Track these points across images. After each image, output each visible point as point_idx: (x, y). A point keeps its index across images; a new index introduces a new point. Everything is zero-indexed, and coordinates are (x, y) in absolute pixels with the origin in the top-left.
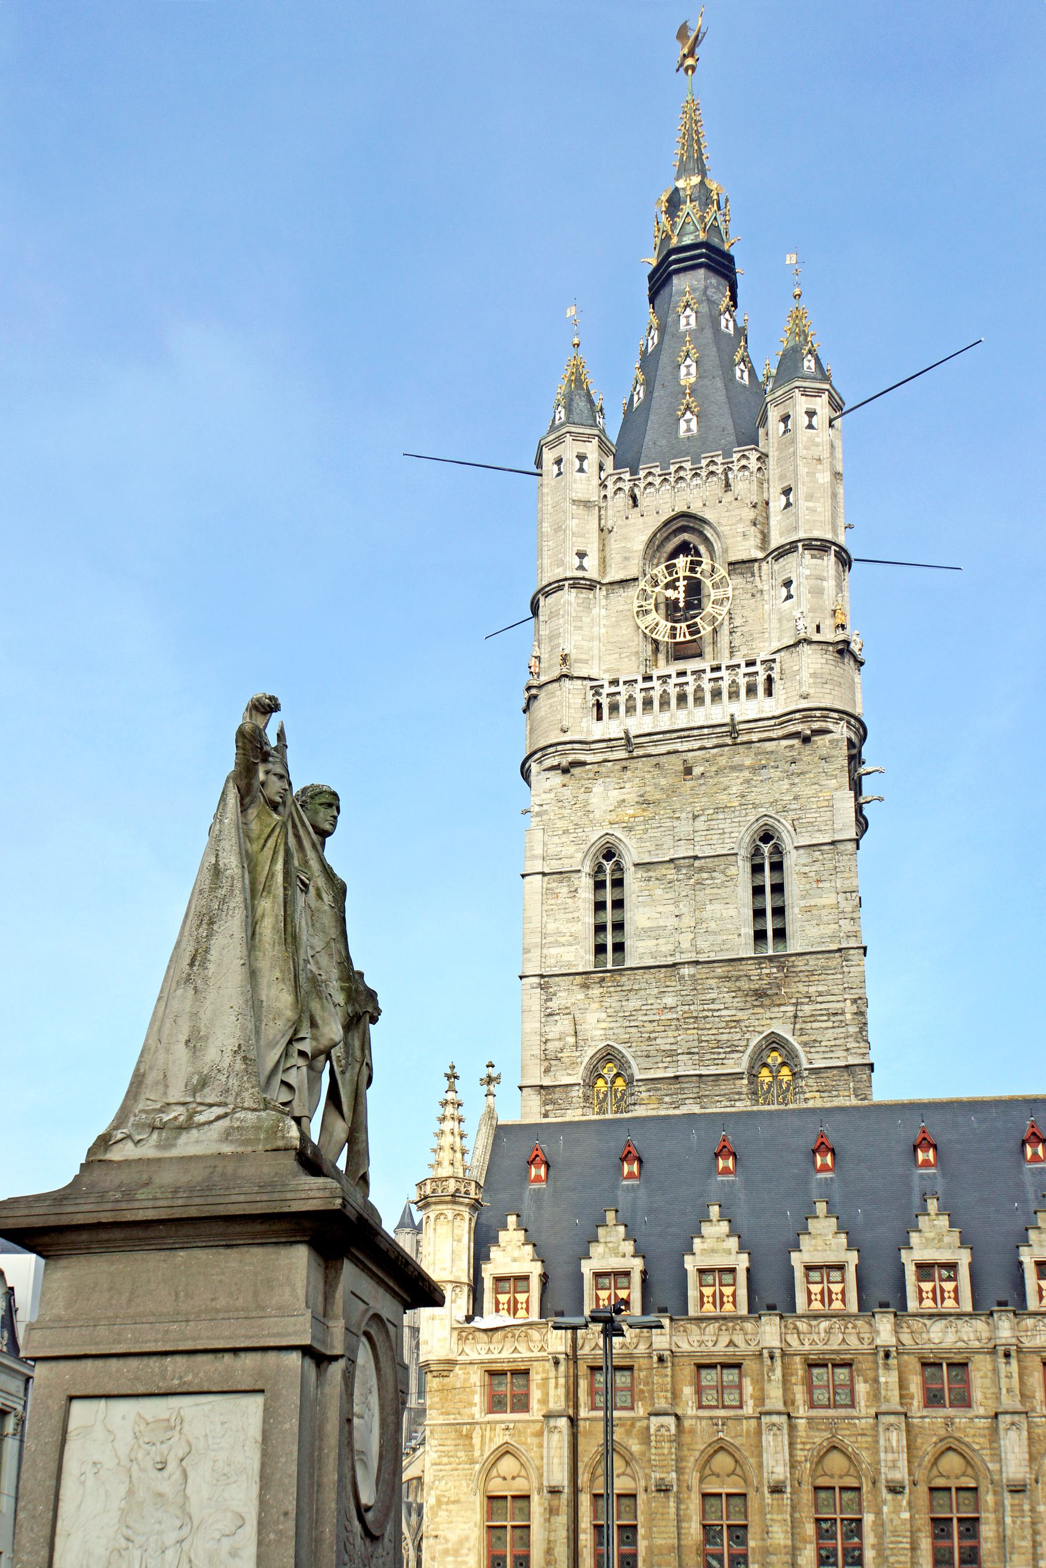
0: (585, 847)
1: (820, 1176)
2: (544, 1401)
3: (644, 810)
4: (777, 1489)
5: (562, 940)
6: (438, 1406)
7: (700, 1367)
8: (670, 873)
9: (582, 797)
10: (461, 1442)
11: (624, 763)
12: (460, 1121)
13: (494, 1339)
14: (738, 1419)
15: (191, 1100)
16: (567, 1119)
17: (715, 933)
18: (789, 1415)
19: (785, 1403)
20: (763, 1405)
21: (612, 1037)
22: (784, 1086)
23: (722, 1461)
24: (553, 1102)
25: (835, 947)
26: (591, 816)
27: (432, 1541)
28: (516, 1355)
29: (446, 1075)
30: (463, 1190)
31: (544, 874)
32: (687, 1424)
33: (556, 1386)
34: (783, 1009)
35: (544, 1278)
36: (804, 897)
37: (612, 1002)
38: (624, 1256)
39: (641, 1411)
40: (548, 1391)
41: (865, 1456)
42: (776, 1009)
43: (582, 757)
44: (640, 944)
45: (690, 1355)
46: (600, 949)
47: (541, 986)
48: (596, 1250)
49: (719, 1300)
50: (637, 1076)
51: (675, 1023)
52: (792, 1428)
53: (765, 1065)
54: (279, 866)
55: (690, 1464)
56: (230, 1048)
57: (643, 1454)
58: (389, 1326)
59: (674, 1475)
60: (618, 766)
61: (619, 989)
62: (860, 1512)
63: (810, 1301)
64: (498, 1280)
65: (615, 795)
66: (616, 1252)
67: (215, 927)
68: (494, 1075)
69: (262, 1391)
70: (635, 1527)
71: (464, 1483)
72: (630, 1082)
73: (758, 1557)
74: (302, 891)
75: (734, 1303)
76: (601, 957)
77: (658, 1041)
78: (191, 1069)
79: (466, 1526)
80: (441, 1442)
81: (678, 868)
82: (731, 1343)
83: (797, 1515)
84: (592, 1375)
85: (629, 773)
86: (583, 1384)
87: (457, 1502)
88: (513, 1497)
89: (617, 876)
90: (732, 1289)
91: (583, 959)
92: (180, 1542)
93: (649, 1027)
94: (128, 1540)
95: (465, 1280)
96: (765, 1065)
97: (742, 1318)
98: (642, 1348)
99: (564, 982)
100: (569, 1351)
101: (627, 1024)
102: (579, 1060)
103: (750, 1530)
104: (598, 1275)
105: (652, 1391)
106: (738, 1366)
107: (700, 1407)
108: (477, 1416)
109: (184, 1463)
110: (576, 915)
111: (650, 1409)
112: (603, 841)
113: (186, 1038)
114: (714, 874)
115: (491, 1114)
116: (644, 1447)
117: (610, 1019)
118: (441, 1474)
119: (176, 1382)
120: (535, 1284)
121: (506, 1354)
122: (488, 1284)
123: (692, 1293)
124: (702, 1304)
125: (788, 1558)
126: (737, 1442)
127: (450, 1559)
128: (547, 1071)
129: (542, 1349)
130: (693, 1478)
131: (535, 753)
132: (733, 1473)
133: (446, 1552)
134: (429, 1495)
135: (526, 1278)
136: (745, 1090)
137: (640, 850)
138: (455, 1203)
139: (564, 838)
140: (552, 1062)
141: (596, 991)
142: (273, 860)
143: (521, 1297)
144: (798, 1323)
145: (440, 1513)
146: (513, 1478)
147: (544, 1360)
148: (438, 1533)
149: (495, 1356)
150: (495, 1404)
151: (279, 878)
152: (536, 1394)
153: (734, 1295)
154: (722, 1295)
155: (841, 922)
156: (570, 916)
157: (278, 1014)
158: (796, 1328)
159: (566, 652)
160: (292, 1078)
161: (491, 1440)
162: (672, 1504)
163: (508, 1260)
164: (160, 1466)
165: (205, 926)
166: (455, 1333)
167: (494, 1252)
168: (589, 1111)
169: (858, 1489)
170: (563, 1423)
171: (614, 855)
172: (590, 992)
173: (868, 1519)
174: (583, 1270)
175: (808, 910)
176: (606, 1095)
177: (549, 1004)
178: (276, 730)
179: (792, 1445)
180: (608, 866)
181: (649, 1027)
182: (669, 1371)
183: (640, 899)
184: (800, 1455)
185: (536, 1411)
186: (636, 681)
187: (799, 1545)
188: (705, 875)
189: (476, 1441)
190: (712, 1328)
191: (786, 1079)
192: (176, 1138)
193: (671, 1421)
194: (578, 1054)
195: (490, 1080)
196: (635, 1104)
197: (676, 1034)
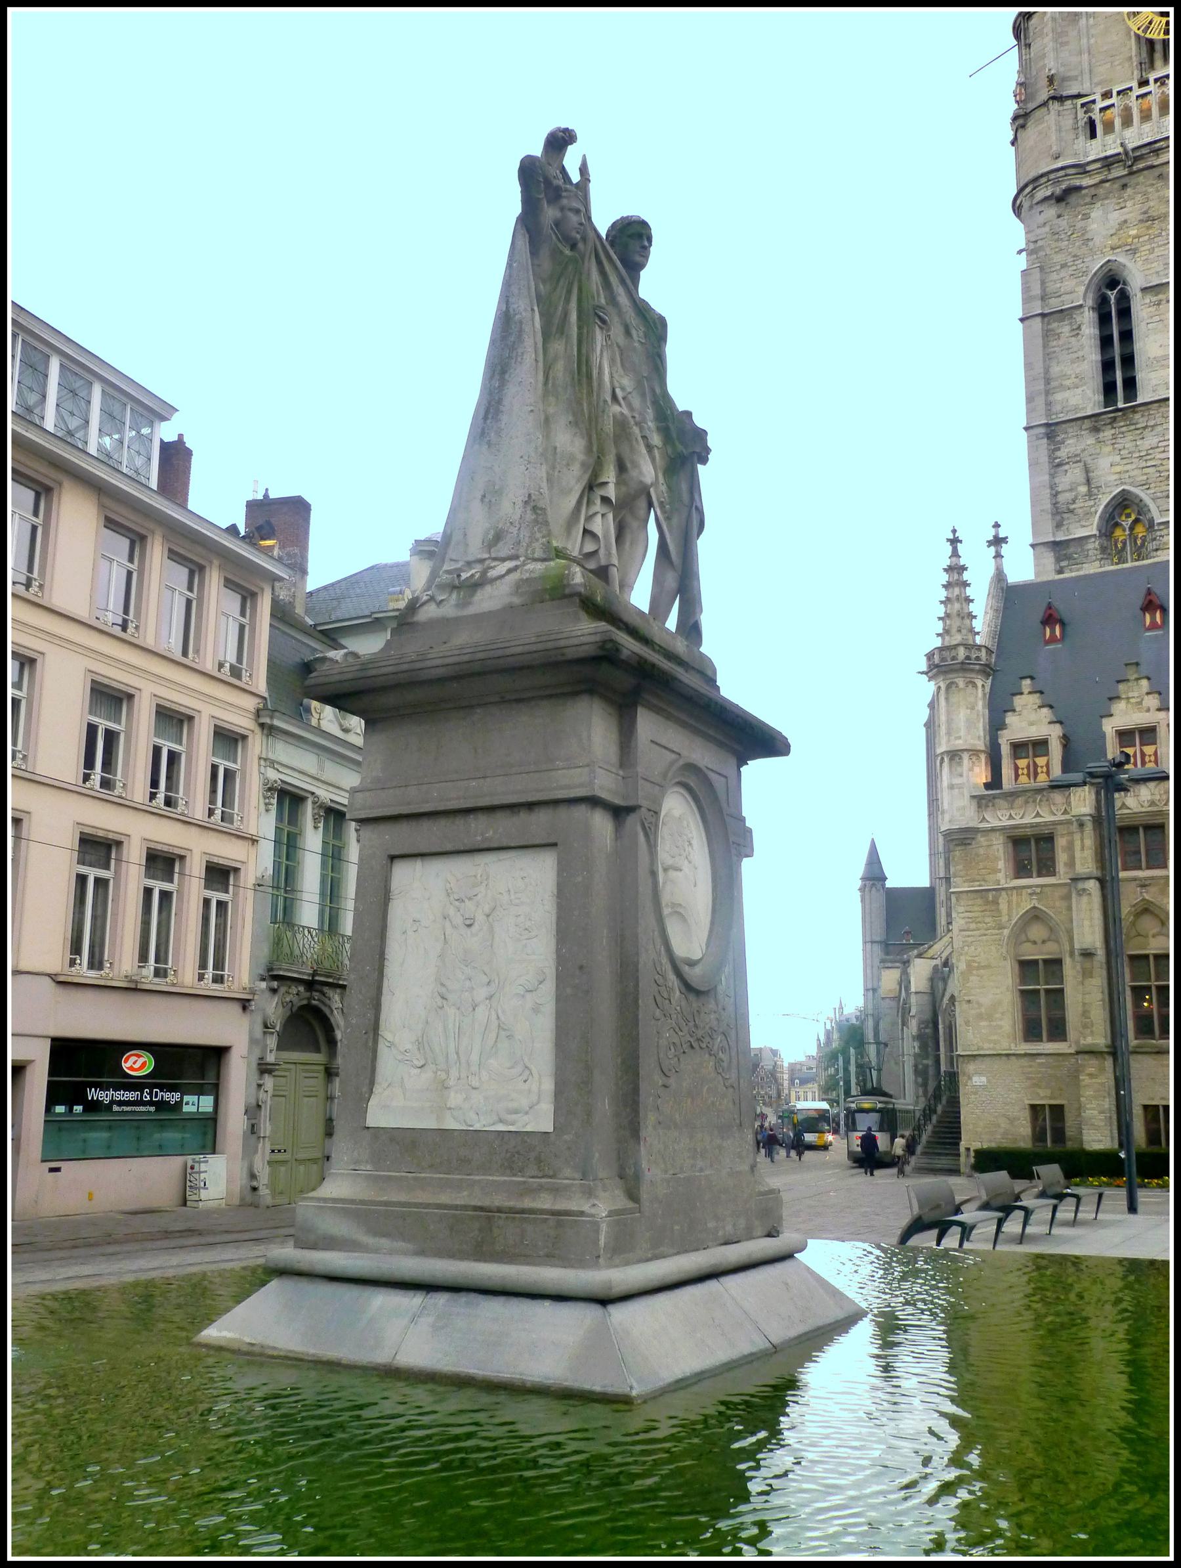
0: (1087, 280)
2: (1071, 863)
3: (1148, 228)
5: (1067, 383)
6: (962, 873)
9: (1079, 225)
10: (988, 907)
11: (1124, 181)
13: (1015, 805)
15: (487, 556)
16: (1081, 573)
21: (1128, 481)
24: (1068, 557)
26: (1090, 243)
27: (965, 1006)
28: (1038, 820)
29: (948, 540)
33: (1083, 849)
35: (1066, 740)
37: (1127, 442)
38: (1148, 710)
40: (1079, 854)
43: (1077, 183)
44: (1153, 375)
54: (573, 305)
56: (520, 499)
58: (712, 775)
60: (1117, 186)
61: (1133, 427)
65: (1115, 217)
67: (507, 376)
69: (555, 845)
71: (993, 948)
74: (601, 328)
78: (487, 525)
79: (998, 991)
80: (968, 909)
85: (1129, 191)
88: (1045, 961)
92: (490, 998)
94: (443, 998)
95: (983, 748)
99: (1072, 430)
101: (1144, 464)
102: (1093, 509)
108: (1003, 881)
109: (490, 919)
110: (1080, 354)
112: (1105, 269)
113: (482, 493)
115: (1000, 576)
117: (1125, 461)
118: (970, 939)
119: (479, 838)
121: (1028, 820)
122: (1005, 750)
127: (983, 1023)
128: (1059, 526)
129: (1065, 812)
131: (1026, 186)
133: (980, 1017)
134: (959, 960)
137: (1147, 272)
138: (965, 670)
139: (1063, 273)
140: (1065, 516)
141: (1108, 433)
142: (568, 300)
143: (1041, 761)
145: (972, 978)
146: (1044, 942)
147: (1069, 822)
148: (971, 998)
149: (1017, 821)
150: (1021, 870)
151: (574, 317)
152: (1061, 858)
156: (1076, 355)
157: (571, 458)
159: (1052, 72)
160: (597, 526)
161: (1018, 905)
163: (1024, 724)
164: (468, 922)
165: (497, 377)
167: (1010, 719)
170: (1092, 886)
172: (1101, 435)
174: (1104, 728)
176: (1124, 543)
178: (578, 164)
183: (1150, 326)
185: (1062, 875)
186: (1130, 89)
189: (1003, 906)
192: (472, 595)
194: (1092, 503)
196: (1157, 550)
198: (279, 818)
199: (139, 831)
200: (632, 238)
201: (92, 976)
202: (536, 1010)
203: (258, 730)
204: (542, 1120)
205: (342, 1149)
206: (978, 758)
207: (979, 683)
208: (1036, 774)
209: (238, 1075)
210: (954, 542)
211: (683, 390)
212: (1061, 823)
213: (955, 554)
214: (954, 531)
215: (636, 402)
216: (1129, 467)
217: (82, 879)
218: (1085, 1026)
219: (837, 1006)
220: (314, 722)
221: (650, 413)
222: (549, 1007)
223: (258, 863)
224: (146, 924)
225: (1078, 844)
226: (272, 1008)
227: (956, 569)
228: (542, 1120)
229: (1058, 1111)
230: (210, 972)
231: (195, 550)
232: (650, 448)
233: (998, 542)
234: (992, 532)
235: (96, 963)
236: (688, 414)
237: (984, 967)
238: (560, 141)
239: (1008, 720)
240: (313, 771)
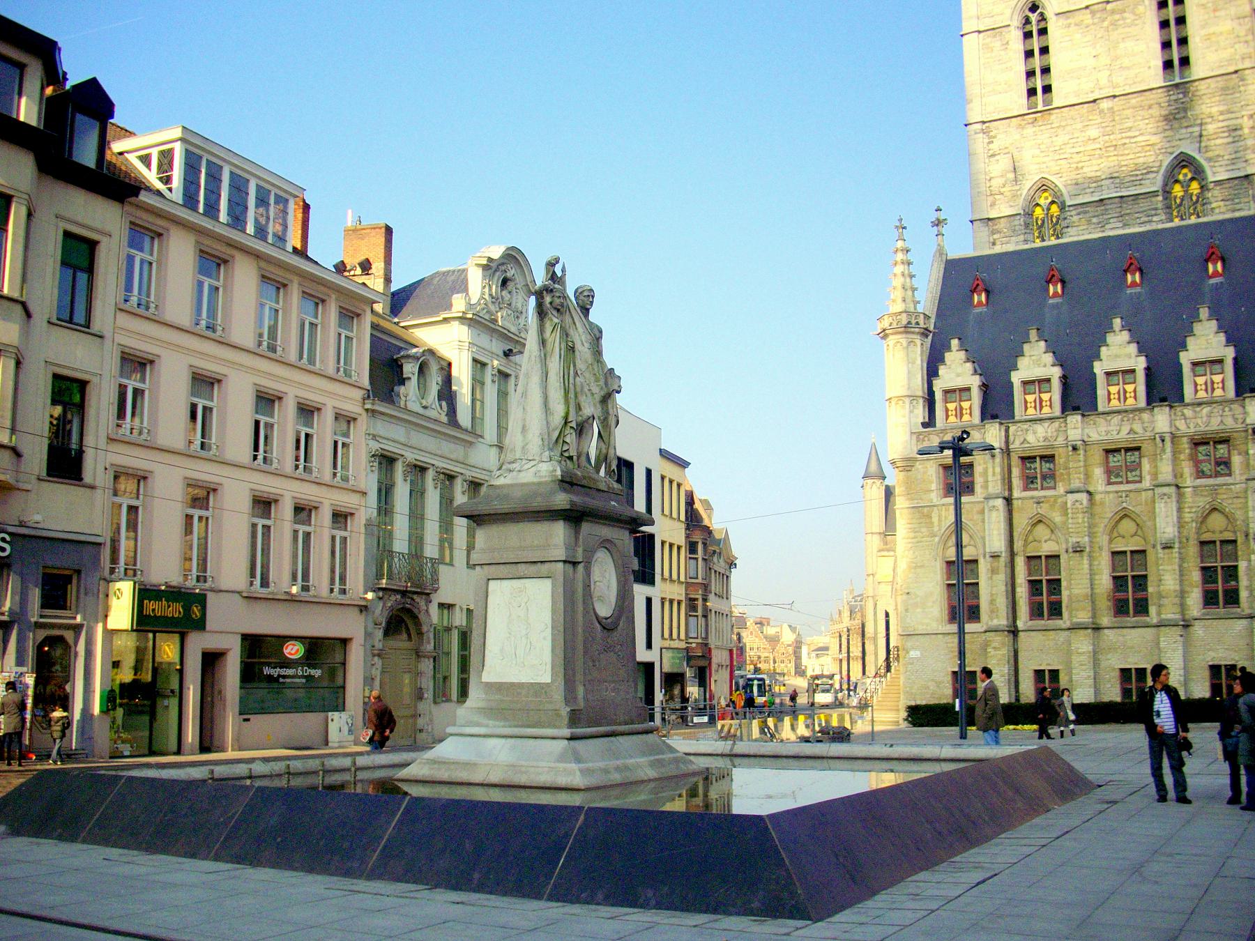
1: (1213, 281)
2: (985, 487)
4: (1167, 547)
7: (1108, 451)
8: (1086, 17)
12: (909, 264)
14: (1138, 491)
17: (1128, 68)
18: (1177, 486)
19: (1175, 476)
20: (1156, 478)
22: (1194, 198)
23: (1127, 526)
25: (1231, 69)
30: (913, 322)
31: (979, 32)
32: (1098, 497)
33: (994, 474)
34: (1190, 130)
36: (1203, 27)
39: (1061, 489)
41: (1239, 515)
42: (1184, 131)
45: (1098, 443)
46: (1032, 92)
47: (983, 131)
48: (1022, 363)
49: (1123, 396)
50: (1068, 203)
51: (1098, 152)
52: (1180, 496)
53: (1177, 181)
55: (1100, 528)
57: (1064, 523)
59: (1087, 539)
62: (1236, 560)
63: (1196, 391)
64: (946, 392)
66: (1038, 363)
68: (942, 218)
70: (1059, 580)
72: (1062, 207)
73: (1155, 601)
75: (1135, 398)
76: (1033, 98)
77: (1085, 170)
81: (1093, 13)
82: (1131, 431)
83: (1185, 565)
84: (1023, 463)
86: (1016, 472)
87: (922, 566)
89: (1042, 25)
90: (1221, 376)
91: (1019, 102)
93: (1077, 158)
95: (920, 393)
96: (1177, 181)
97: (1140, 410)
98: (1061, 440)
100: (1003, 446)
103: (1150, 578)
104: (1025, 383)
105: (1069, 474)
106: (1138, 449)
107: (1109, 483)
111: (1068, 488)
114: (1126, 15)
116: (1064, 518)
120: (1056, 385)
122: (938, 396)
123: (1101, 392)
124: (1109, 400)
125: (1177, 600)
126: (1137, 510)
130: (1103, 540)
132: (1135, 534)
135: (1048, 380)
136: (1160, 205)
144: (1185, 411)
152: (978, 480)
153: (1135, 391)
154: (1125, 392)
155: (1237, 46)
158: (1183, 415)
160: (568, 440)
162: (1086, 561)
163: (953, 375)
166: (914, 437)
167: (942, 370)
168: (1030, 237)
169: (1234, 542)
170: (1000, 503)
171: (1038, 7)
172: (1025, 132)
173: (1242, 565)
174: (1013, 379)
175: (1208, 38)
177: (991, 146)
179: (1180, 510)
180: (1034, 17)
181: (1077, 158)
182: (1081, 457)
184: (1187, 517)
187: (1187, 589)
188: (1117, 17)
189: (935, 520)
190: (1116, 419)
191: (1196, 192)
193: (1083, 497)
195: (938, 223)
197: (1099, 161)
198: (380, 474)
199: (289, 492)
200: (585, 301)
201: (263, 592)
203: (364, 413)
208: (962, 415)
209: (356, 658)
211: (610, 359)
215: (587, 375)
216: (1046, 159)
217: (254, 526)
218: (992, 611)
220: (402, 404)
222: (550, 637)
223: (366, 509)
224: (295, 556)
225: (990, 470)
226: (380, 612)
228: (547, 679)
229: (1054, 674)
230: (337, 587)
231: (318, 291)
235: (265, 583)
240: (402, 440)
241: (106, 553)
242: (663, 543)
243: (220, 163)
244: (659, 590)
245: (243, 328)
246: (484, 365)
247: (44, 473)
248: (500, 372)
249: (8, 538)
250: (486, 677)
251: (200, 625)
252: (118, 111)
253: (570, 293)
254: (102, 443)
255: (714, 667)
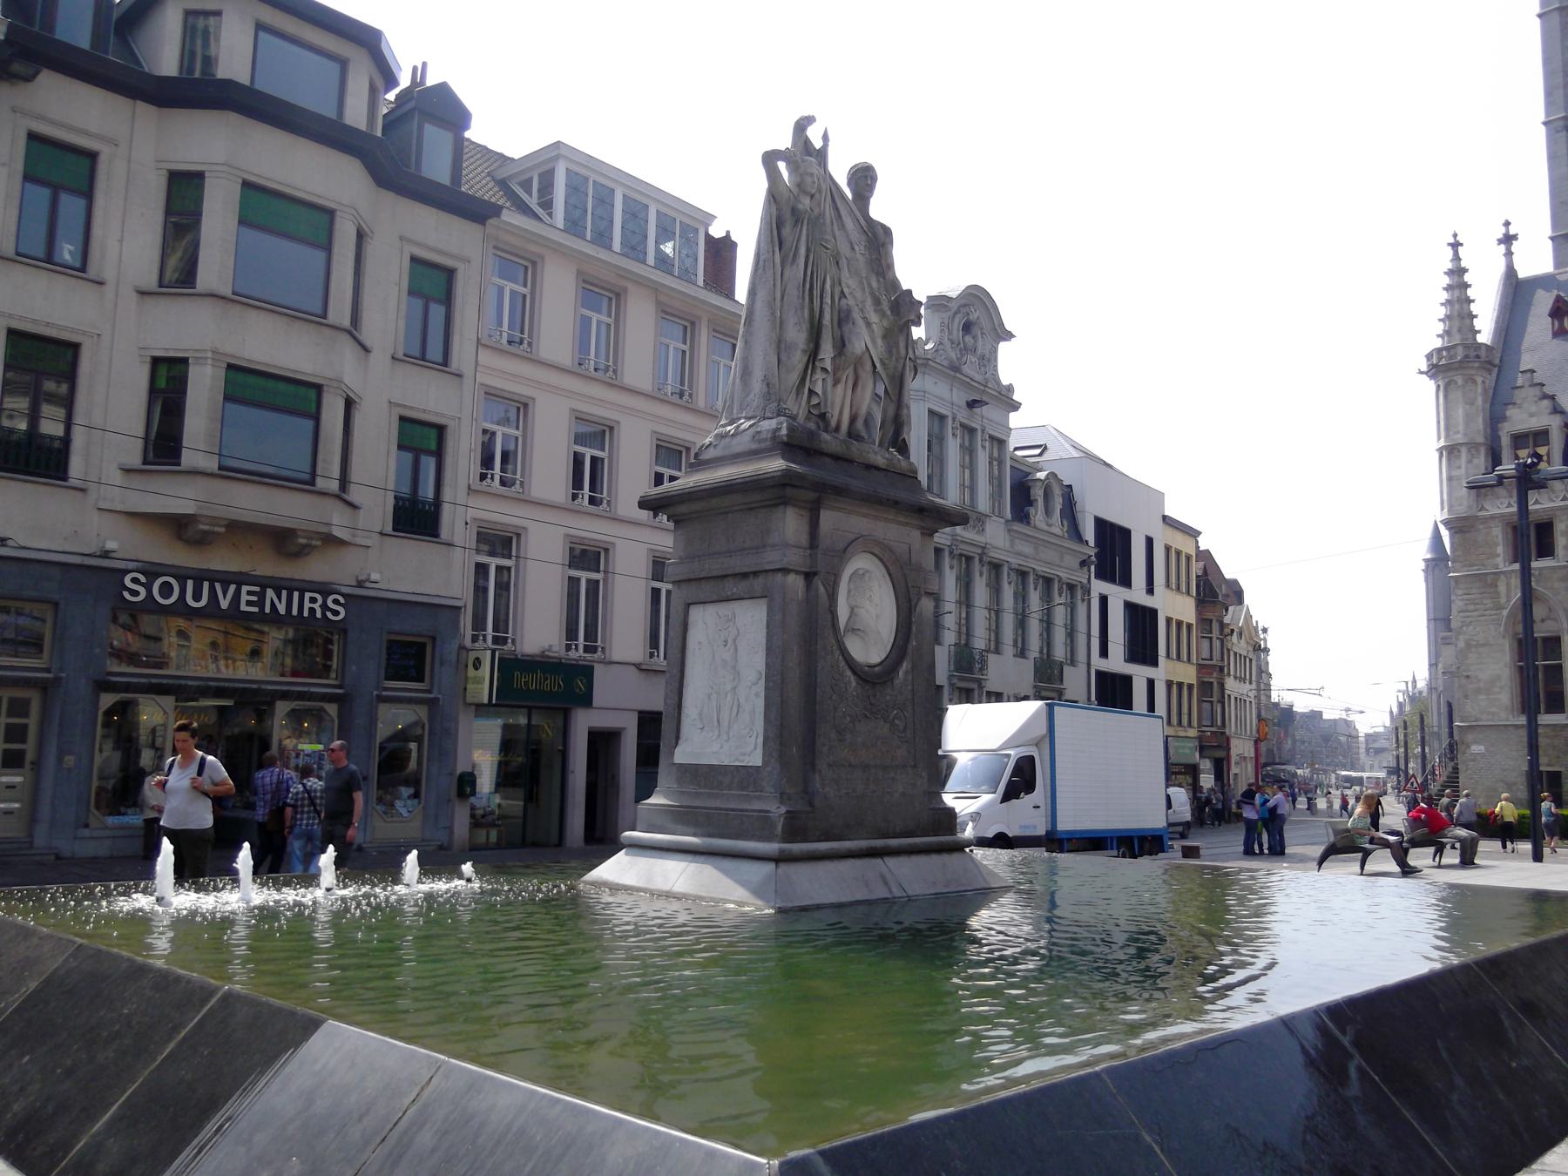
95: (1481, 439)
115: (1510, 272)
122: (1505, 441)
167: (1511, 412)
189: (1502, 588)
202: (757, 695)
204: (756, 760)
205: (664, 777)
206: (1478, 450)
207: (1479, 380)
210: (1455, 245)
212: (1559, 508)
213: (1456, 258)
214: (1455, 236)
219: (1410, 679)
221: (869, 302)
227: (1457, 272)
228: (756, 760)
232: (868, 324)
233: (1508, 239)
234: (1503, 230)
236: (910, 292)
237: (1483, 645)
238: (802, 125)
239: (1508, 413)
241: (466, 621)
242: (1169, 620)
243: (645, 201)
244: (1162, 672)
245: (638, 365)
246: (942, 418)
247: (389, 529)
248: (963, 426)
249: (342, 600)
250: (682, 755)
251: (586, 700)
252: (474, 123)
253: (841, 179)
254: (461, 496)
255: (1234, 759)
